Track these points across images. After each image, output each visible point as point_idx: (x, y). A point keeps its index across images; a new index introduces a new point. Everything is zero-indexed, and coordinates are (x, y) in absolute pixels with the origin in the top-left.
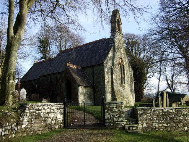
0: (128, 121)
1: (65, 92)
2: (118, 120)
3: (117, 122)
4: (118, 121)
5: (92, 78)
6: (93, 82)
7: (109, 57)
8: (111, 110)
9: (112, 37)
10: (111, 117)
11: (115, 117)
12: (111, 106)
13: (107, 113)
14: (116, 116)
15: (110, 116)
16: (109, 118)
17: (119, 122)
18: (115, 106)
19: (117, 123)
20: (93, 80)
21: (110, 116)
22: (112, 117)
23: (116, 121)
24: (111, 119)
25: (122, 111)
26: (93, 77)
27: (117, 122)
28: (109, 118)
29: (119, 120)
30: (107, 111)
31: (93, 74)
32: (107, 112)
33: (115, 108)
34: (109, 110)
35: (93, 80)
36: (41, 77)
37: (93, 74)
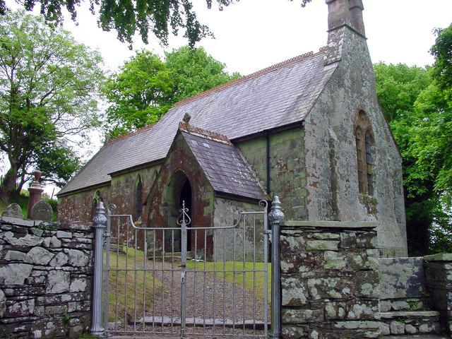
0: (396, 318)
1: (172, 216)
2: (347, 313)
3: (341, 320)
4: (345, 319)
5: (264, 174)
6: (268, 185)
7: (350, 261)
8: (312, 265)
9: (331, 45)
10: (310, 297)
11: (332, 299)
12: (313, 244)
13: (293, 276)
14: (338, 295)
15: (308, 290)
16: (304, 301)
17: (350, 325)
18: (332, 245)
19: (343, 329)
20: (269, 179)
21: (308, 290)
22: (318, 297)
23: (338, 319)
24: (309, 305)
25: (368, 269)
26: (269, 168)
27: (339, 325)
28: (304, 301)
29: (351, 315)
30: (292, 266)
31: (268, 158)
32: (293, 272)
33: (330, 255)
34: (300, 262)
35: (269, 179)
36: (112, 175)
37: (268, 158)
